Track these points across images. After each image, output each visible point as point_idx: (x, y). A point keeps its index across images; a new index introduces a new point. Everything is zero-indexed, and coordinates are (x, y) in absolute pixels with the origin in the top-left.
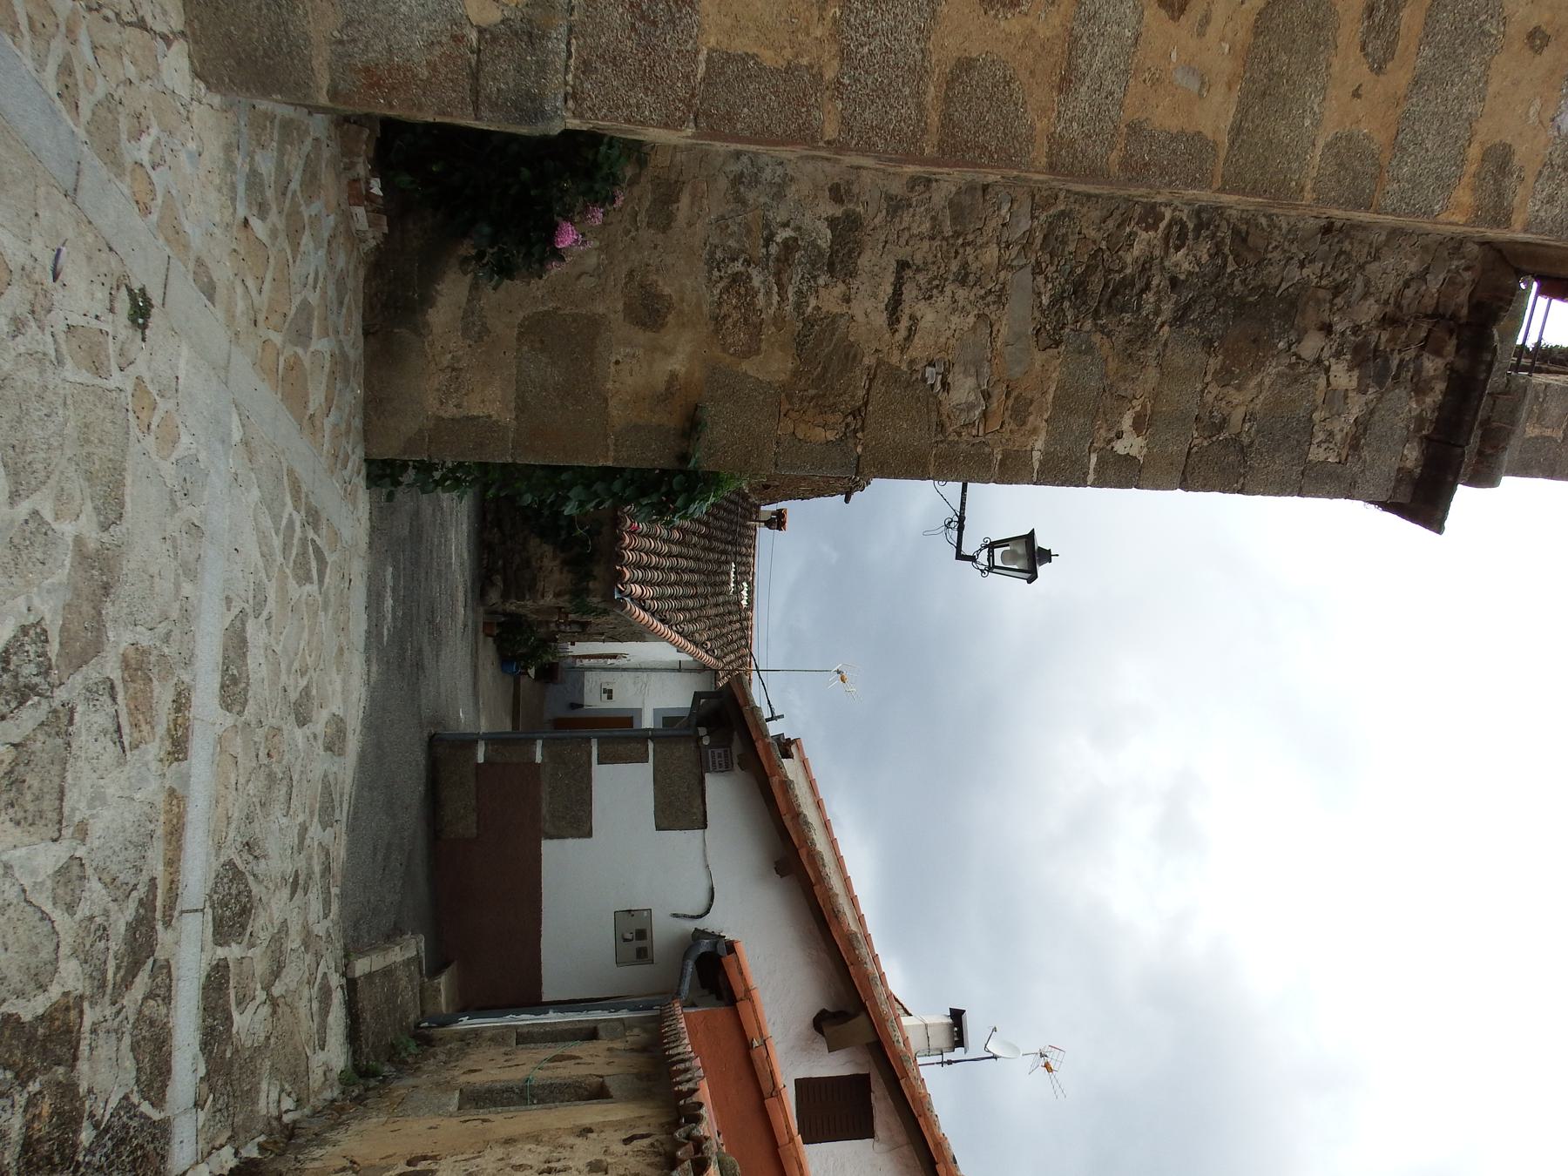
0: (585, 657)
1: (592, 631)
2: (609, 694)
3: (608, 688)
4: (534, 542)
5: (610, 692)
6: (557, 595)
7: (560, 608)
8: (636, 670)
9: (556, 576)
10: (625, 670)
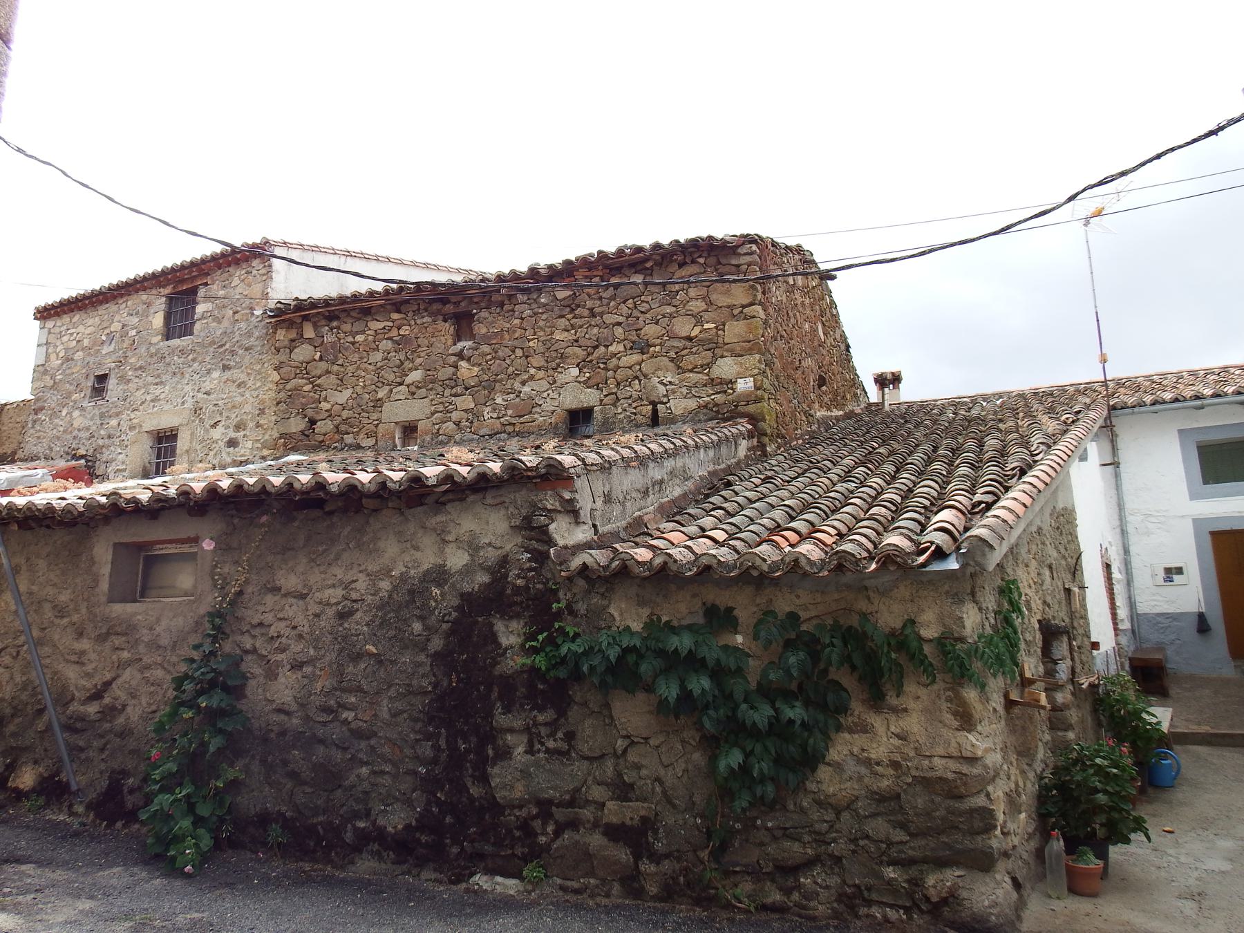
0: (1114, 615)
1: (1063, 614)
2: (1171, 573)
3: (1162, 574)
4: (827, 782)
5: (1169, 571)
6: (967, 721)
7: (1009, 704)
8: (1124, 533)
9: (913, 723)
10: (1126, 551)
